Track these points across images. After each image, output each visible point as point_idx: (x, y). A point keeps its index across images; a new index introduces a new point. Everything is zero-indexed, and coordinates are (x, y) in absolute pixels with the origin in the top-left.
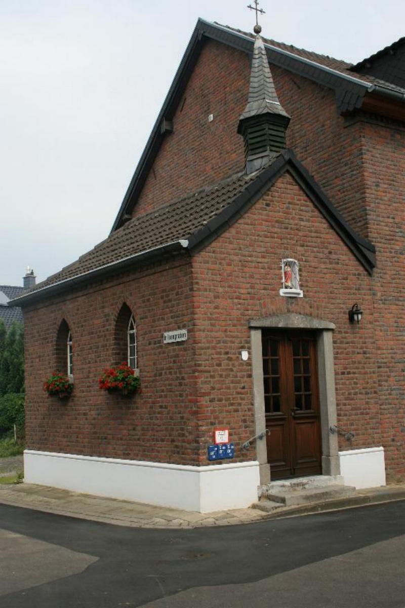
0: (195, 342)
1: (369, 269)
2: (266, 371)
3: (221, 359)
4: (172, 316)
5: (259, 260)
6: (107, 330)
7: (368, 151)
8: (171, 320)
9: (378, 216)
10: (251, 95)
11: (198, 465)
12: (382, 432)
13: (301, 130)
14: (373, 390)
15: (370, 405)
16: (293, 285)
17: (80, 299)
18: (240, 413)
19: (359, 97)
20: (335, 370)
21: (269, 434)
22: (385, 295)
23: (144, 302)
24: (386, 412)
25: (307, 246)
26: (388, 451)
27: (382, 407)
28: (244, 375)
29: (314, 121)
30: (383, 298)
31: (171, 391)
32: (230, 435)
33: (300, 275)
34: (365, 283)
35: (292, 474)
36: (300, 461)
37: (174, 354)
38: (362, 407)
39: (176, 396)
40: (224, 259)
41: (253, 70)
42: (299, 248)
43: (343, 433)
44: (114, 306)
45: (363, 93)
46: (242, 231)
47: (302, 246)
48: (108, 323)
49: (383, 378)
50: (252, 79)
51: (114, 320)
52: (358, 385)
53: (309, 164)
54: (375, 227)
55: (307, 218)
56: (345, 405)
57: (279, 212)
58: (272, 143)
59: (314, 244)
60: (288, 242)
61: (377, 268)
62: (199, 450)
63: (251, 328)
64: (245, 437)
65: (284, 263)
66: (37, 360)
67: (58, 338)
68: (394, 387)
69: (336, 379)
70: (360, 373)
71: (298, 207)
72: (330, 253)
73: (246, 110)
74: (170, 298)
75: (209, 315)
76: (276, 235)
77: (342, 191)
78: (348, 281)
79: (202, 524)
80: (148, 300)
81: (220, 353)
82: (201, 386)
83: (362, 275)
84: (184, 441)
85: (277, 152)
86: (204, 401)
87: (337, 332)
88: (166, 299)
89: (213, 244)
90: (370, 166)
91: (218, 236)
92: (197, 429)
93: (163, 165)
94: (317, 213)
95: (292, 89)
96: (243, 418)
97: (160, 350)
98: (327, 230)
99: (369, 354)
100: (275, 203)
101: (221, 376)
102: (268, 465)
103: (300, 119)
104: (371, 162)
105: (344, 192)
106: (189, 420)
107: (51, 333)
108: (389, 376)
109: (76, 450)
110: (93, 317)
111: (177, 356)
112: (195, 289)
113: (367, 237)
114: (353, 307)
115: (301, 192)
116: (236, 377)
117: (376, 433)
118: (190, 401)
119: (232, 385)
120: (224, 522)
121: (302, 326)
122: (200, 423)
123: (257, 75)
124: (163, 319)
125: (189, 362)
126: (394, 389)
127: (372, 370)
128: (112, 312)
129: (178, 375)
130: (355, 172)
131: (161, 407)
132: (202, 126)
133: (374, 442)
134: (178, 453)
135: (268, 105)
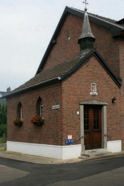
5: (84, 83)
7: (121, 49)
11: (62, 146)
32: (73, 136)
33: (97, 88)
35: (92, 148)
41: (84, 23)
42: (97, 80)
47: (98, 79)
50: (83, 26)
53: (101, 53)
56: (110, 128)
63: (80, 104)
69: (107, 120)
71: (97, 67)
72: (107, 81)
73: (81, 36)
85: (91, 49)
86: (65, 127)
88: (53, 96)
92: (62, 135)
94: (103, 69)
101: (70, 119)
110: (29, 101)
111: (56, 113)
113: (119, 76)
118: (60, 127)
120: (70, 162)
122: (63, 133)
123: (85, 24)
128: (35, 99)
131: (51, 128)
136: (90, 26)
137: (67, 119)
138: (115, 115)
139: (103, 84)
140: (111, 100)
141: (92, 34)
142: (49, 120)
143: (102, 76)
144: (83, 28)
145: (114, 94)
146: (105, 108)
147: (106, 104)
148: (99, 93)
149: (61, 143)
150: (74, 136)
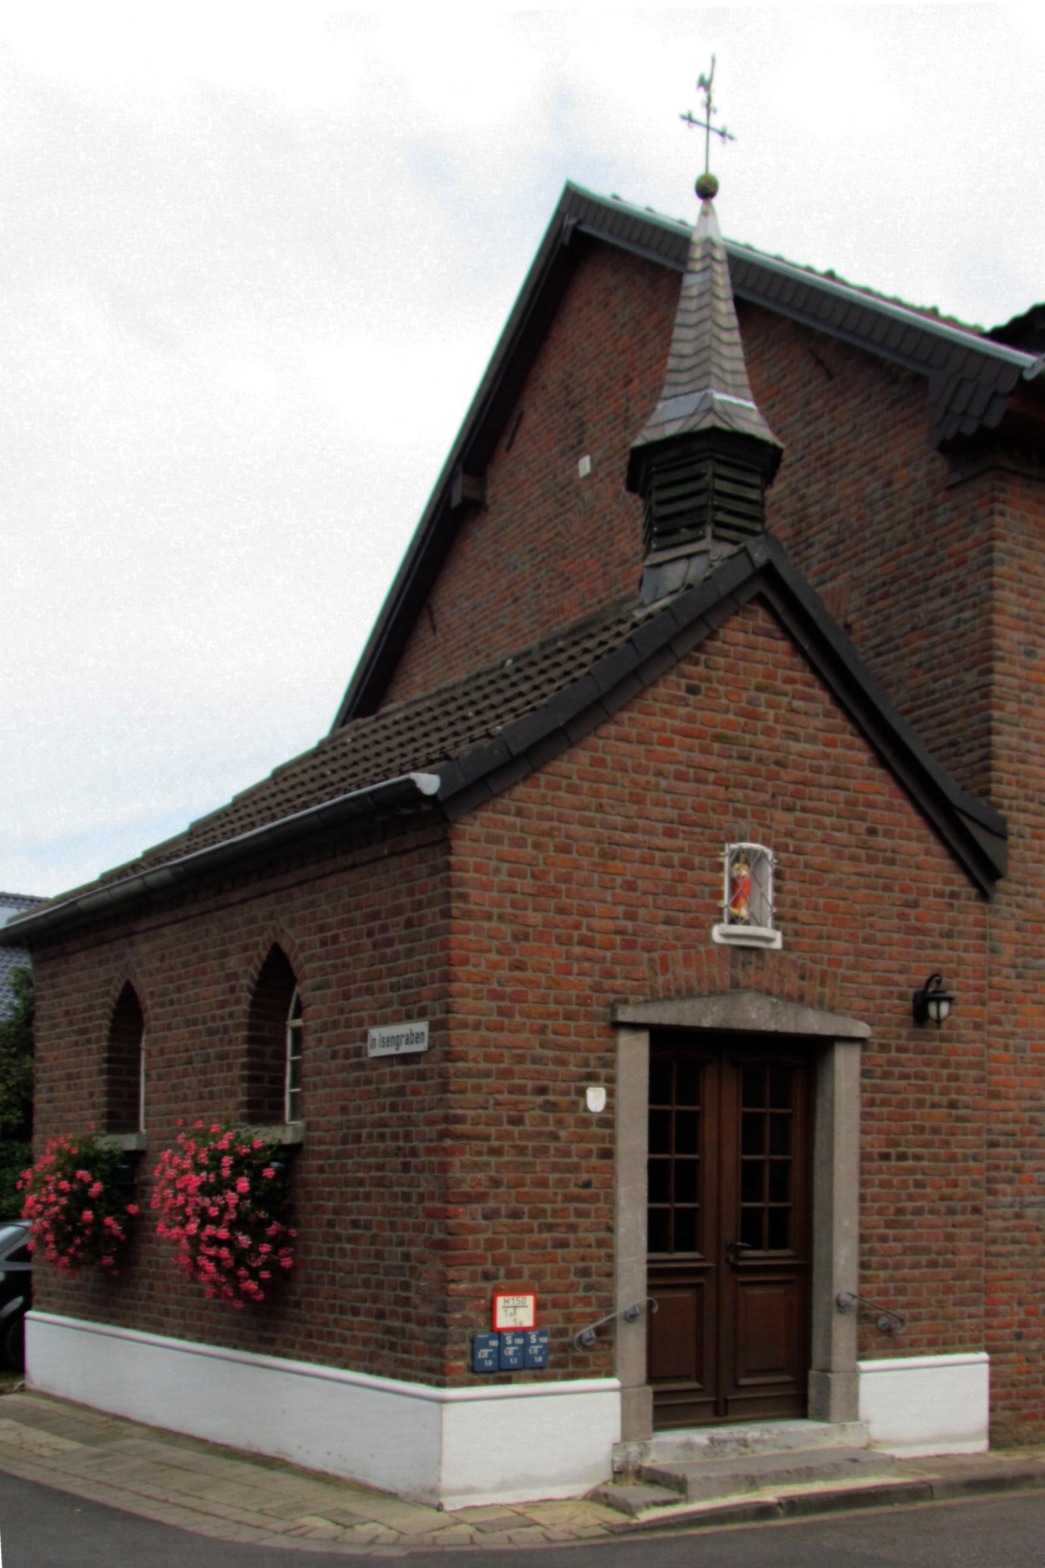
0: (449, 1057)
1: (982, 880)
2: (657, 1141)
3: (521, 1107)
4: (392, 985)
5: (659, 841)
6: (231, 1015)
7: (1011, 554)
8: (390, 994)
9: (1025, 737)
10: (671, 377)
11: (441, 1384)
12: (988, 1314)
13: (828, 496)
14: (969, 1204)
15: (958, 1244)
16: (751, 914)
17: (166, 931)
18: (572, 1251)
19: (995, 394)
20: (862, 1148)
21: (655, 1310)
22: (1024, 954)
23: (324, 943)
24: (1002, 1261)
25: (804, 810)
26: (1002, 1362)
27: (994, 1248)
28: (591, 1151)
29: (865, 469)
30: (1020, 961)
31: (382, 1185)
32: (539, 1306)
33: (777, 889)
34: (971, 918)
35: (721, 1410)
36: (744, 1381)
37: (394, 1085)
38: (934, 1246)
39: (394, 1197)
40: (549, 834)
41: (683, 304)
42: (779, 814)
43: (874, 1312)
44: (249, 953)
45: (1007, 385)
46: (609, 758)
47: (789, 809)
48: (233, 996)
49: (1003, 1174)
50: (678, 333)
51: (249, 990)
52: (928, 1190)
53: (834, 594)
54: (1012, 767)
55: (811, 731)
56: (883, 1239)
57: (727, 711)
58: (721, 517)
59: (824, 805)
60: (746, 796)
61: (1010, 881)
62: (445, 1344)
63: (617, 1026)
64: (583, 1315)
65: (732, 852)
66: (63, 1085)
67: (112, 1030)
68: (1033, 1199)
69: (862, 1172)
70: (935, 1158)
71: (784, 700)
72: (872, 832)
73: (653, 420)
74: (390, 934)
75: (495, 986)
76: (712, 776)
77: (926, 666)
78: (921, 910)
79: (434, 1543)
80: (335, 939)
81: (521, 1090)
82: (459, 1175)
83: (964, 896)
84: (407, 1318)
85: (734, 543)
86: (467, 1215)
87: (876, 1048)
88: (378, 937)
89: (521, 790)
90: (1013, 596)
91: (536, 770)
92: (444, 1290)
93: (457, 597)
94: (839, 720)
95: (810, 382)
96: (581, 1265)
97: (357, 1074)
98: (870, 770)
99: (967, 1107)
100: (715, 685)
101: (522, 1151)
102: (650, 1389)
103: (827, 464)
104: (1016, 585)
105: (931, 669)
106: (424, 1263)
107: (98, 1018)
108: (1018, 1170)
109: (146, 1319)
110: (196, 984)
111: (401, 1091)
112: (455, 912)
113: (987, 793)
114: (929, 982)
115: (798, 660)
116: (567, 1154)
117: (970, 1316)
118: (430, 1214)
119: (553, 1177)
120: (495, 1541)
121: (772, 1026)
122: (452, 1273)
123: (693, 319)
124: (369, 991)
125: (431, 1109)
126: (1032, 1204)
127: (970, 1151)
128: (244, 969)
129: (401, 1143)
130: (967, 615)
131: (355, 1224)
132: (562, 489)
133: (962, 1341)
134: (393, 1347)
135: (718, 407)
136: (736, 337)
137: (496, 1152)
138: (935, 1131)
139: (839, 855)
140: (902, 996)
141: (751, 405)
142: (340, 1155)
143: (825, 779)
144: (676, 348)
145: (935, 946)
146: (845, 1067)
147: (862, 1030)
148: (796, 933)
149: (436, 1361)
150: (555, 1304)
